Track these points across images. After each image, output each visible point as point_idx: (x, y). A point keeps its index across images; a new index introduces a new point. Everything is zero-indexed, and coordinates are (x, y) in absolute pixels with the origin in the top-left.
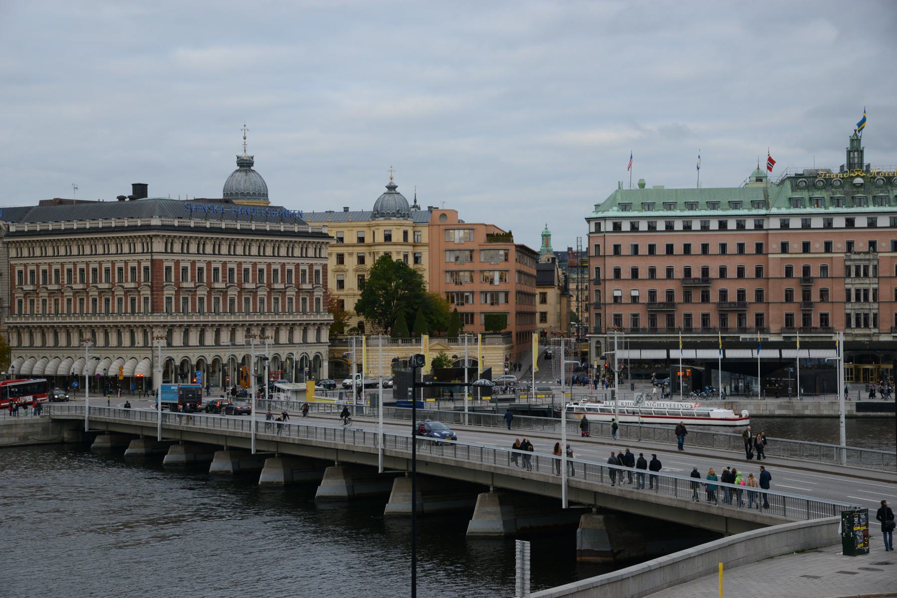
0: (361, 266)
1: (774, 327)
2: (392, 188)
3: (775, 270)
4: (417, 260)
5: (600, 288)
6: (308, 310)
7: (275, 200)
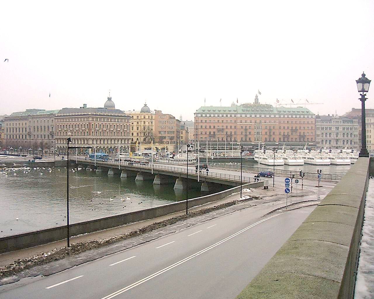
0: (138, 124)
1: (253, 141)
2: (145, 105)
3: (239, 127)
5: (197, 130)
6: (119, 135)
7: (117, 108)
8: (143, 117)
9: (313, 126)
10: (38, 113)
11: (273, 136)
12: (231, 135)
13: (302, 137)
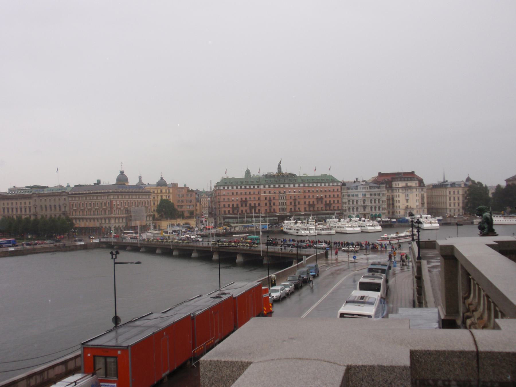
1: (263, 212)
3: (262, 198)
4: (169, 197)
8: (159, 191)
9: (339, 193)
10: (46, 191)
11: (298, 206)
12: (255, 207)
13: (328, 205)
